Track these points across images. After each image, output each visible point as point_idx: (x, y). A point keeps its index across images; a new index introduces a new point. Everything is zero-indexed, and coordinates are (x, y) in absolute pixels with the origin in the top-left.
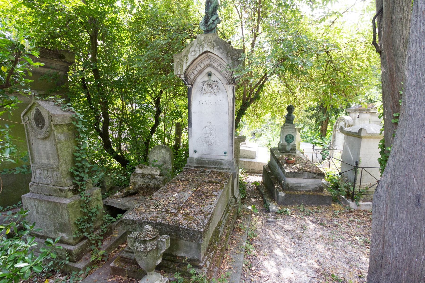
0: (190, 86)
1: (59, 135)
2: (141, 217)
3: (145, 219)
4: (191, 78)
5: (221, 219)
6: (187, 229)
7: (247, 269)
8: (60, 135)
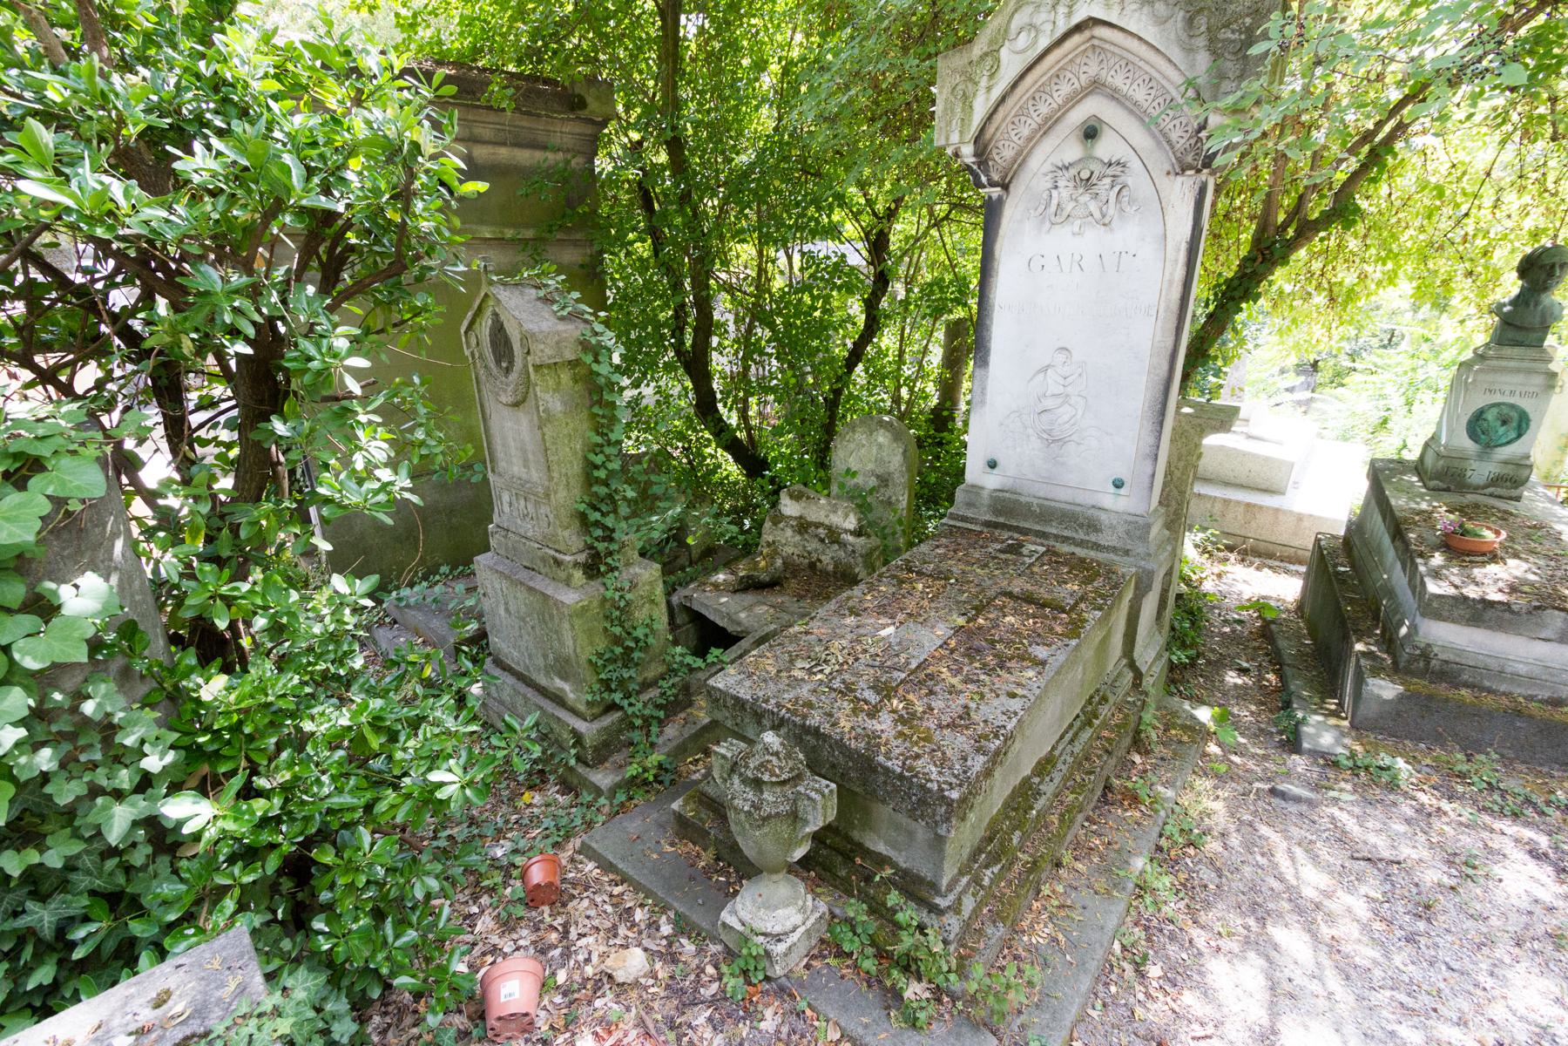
0: (995, 192)
1: (548, 397)
2: (761, 694)
3: (773, 701)
4: (1003, 154)
5: (1054, 748)
6: (901, 777)
7: (1125, 965)
8: (552, 398)
